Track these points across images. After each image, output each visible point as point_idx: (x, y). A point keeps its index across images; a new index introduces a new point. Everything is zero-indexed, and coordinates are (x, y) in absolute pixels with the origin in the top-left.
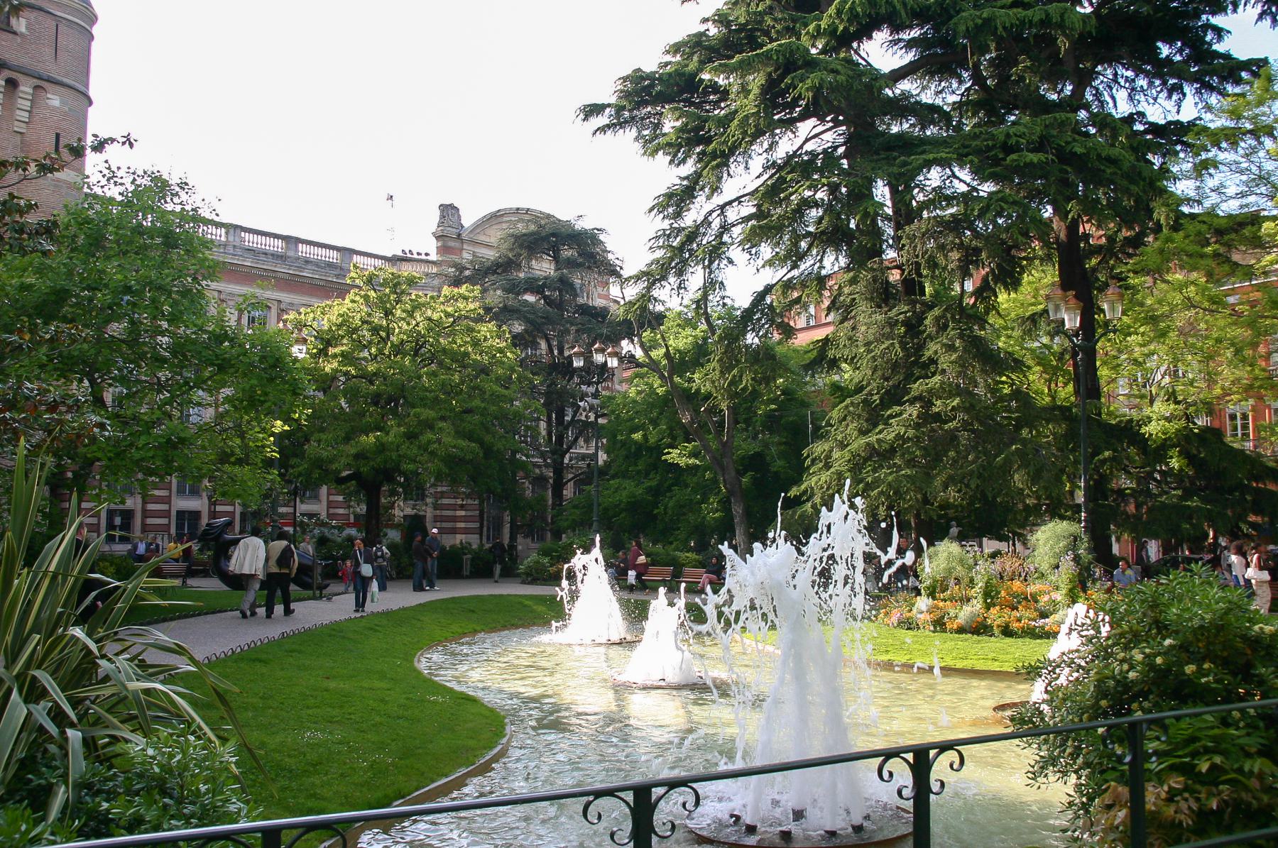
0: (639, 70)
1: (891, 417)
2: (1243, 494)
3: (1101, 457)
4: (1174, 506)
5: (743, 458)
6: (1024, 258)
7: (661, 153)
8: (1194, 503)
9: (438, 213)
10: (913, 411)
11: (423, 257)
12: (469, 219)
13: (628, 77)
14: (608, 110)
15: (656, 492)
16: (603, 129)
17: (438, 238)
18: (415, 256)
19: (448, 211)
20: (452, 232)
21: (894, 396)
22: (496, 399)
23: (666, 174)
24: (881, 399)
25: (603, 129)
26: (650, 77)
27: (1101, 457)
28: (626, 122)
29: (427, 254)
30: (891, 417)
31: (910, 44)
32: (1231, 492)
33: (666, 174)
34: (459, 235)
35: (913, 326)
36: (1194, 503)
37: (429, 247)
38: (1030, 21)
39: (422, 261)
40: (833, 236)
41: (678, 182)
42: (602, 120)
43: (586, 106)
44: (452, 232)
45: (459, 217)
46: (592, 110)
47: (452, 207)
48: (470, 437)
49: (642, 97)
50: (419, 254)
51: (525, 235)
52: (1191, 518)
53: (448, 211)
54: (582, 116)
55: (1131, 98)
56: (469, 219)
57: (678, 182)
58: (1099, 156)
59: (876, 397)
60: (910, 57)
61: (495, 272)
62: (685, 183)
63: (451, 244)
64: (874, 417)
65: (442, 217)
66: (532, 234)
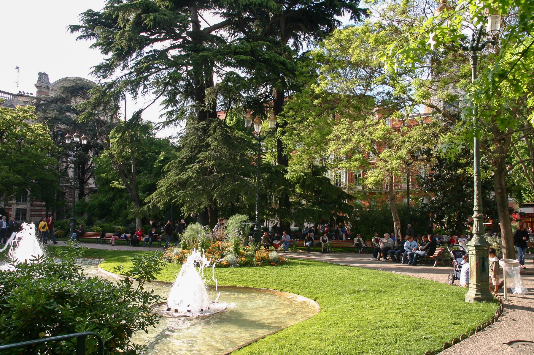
0: (91, 10)
1: (188, 168)
2: (335, 205)
3: (280, 188)
4: (308, 209)
5: (146, 186)
6: (268, 107)
7: (98, 48)
8: (315, 208)
9: (38, 76)
10: (197, 166)
11: (30, 95)
12: (52, 80)
13: (85, 13)
14: (81, 29)
15: (112, 200)
16: (80, 37)
17: (37, 87)
18: (26, 94)
19: (43, 76)
20: (44, 85)
21: (192, 160)
22: (37, 157)
23: (99, 57)
24: (186, 161)
25: (80, 37)
26: (97, 14)
27: (280, 188)
28: (91, 35)
29: (31, 94)
30: (188, 168)
31: (224, 15)
32: (331, 204)
33: (99, 57)
34: (47, 87)
35: (205, 130)
36: (315, 208)
37: (34, 91)
38: (255, 4)
39: (29, 96)
40: (189, 93)
41: (104, 61)
42: (79, 33)
43: (71, 26)
44: (44, 85)
45: (48, 79)
46: (75, 28)
47: (44, 74)
48: (19, 173)
49: (94, 22)
50: (27, 93)
51: (69, 87)
52: (313, 214)
53: (43, 76)
54: (70, 30)
55: (308, 45)
56: (52, 80)
57: (104, 61)
58: (276, 60)
59: (185, 160)
60: (224, 19)
61: (56, 103)
62: (108, 62)
63: (44, 90)
64: (183, 167)
65: (40, 78)
66: (73, 86)
